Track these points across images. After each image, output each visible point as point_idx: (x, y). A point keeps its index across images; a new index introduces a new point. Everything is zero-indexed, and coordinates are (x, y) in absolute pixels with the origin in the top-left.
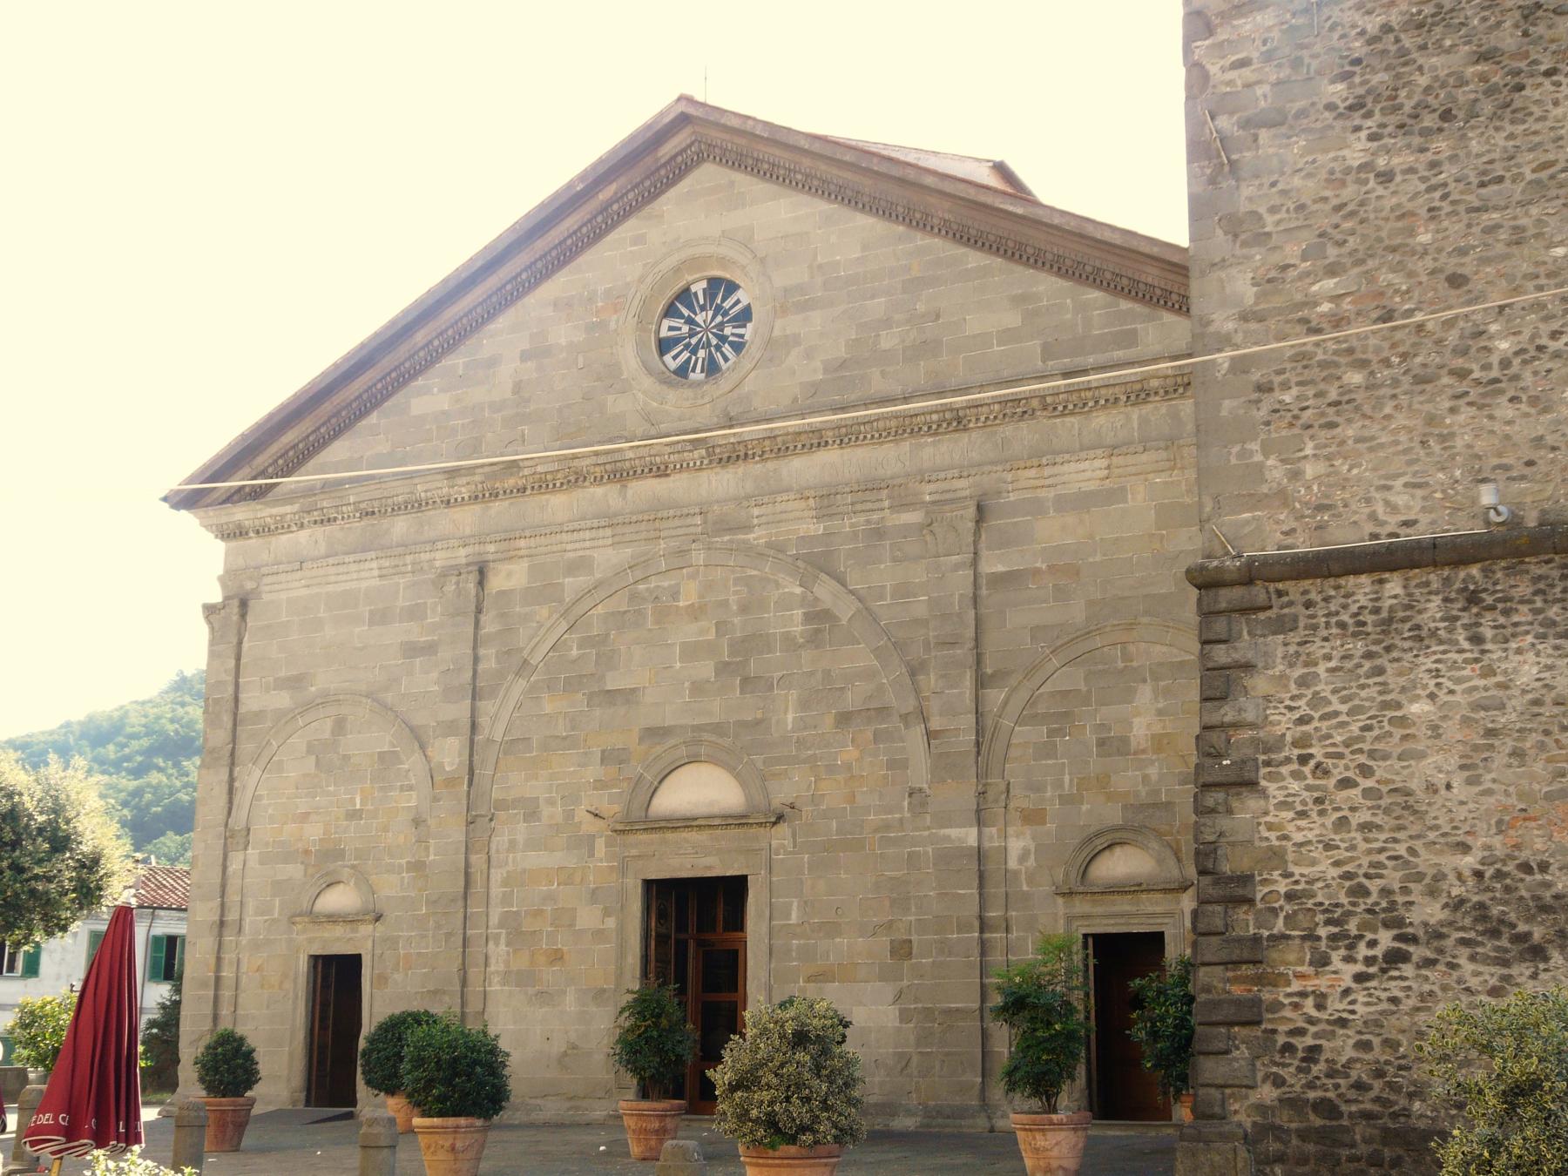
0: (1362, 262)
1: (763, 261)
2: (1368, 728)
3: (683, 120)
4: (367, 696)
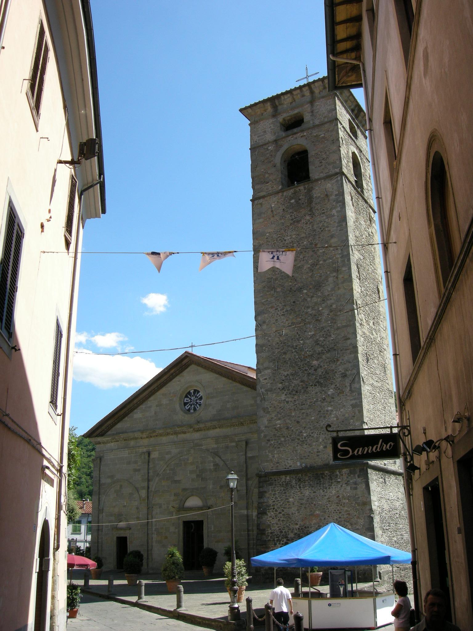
0: (284, 418)
1: (204, 387)
2: (283, 503)
3: (186, 357)
4: (126, 480)
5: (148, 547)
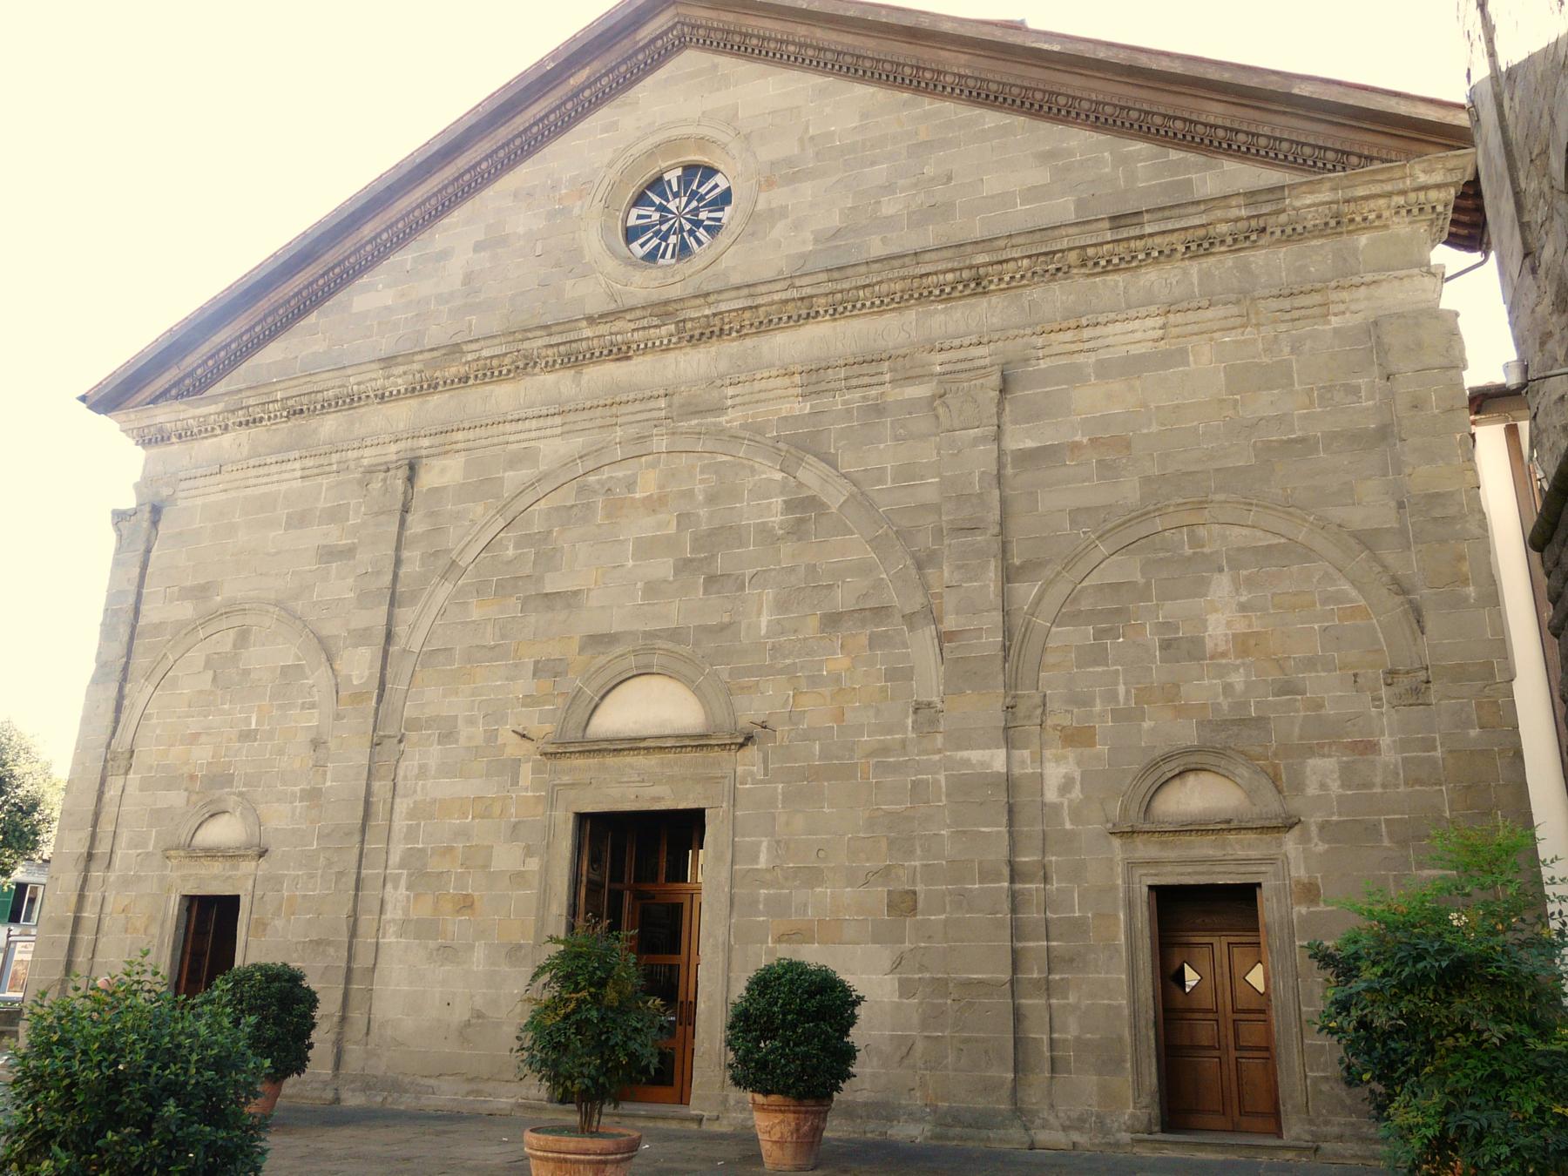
4: (276, 605)
5: (350, 958)
